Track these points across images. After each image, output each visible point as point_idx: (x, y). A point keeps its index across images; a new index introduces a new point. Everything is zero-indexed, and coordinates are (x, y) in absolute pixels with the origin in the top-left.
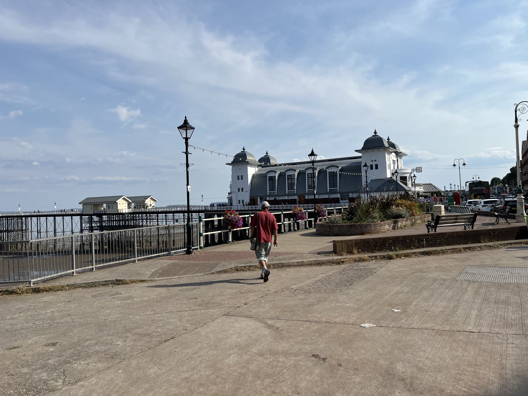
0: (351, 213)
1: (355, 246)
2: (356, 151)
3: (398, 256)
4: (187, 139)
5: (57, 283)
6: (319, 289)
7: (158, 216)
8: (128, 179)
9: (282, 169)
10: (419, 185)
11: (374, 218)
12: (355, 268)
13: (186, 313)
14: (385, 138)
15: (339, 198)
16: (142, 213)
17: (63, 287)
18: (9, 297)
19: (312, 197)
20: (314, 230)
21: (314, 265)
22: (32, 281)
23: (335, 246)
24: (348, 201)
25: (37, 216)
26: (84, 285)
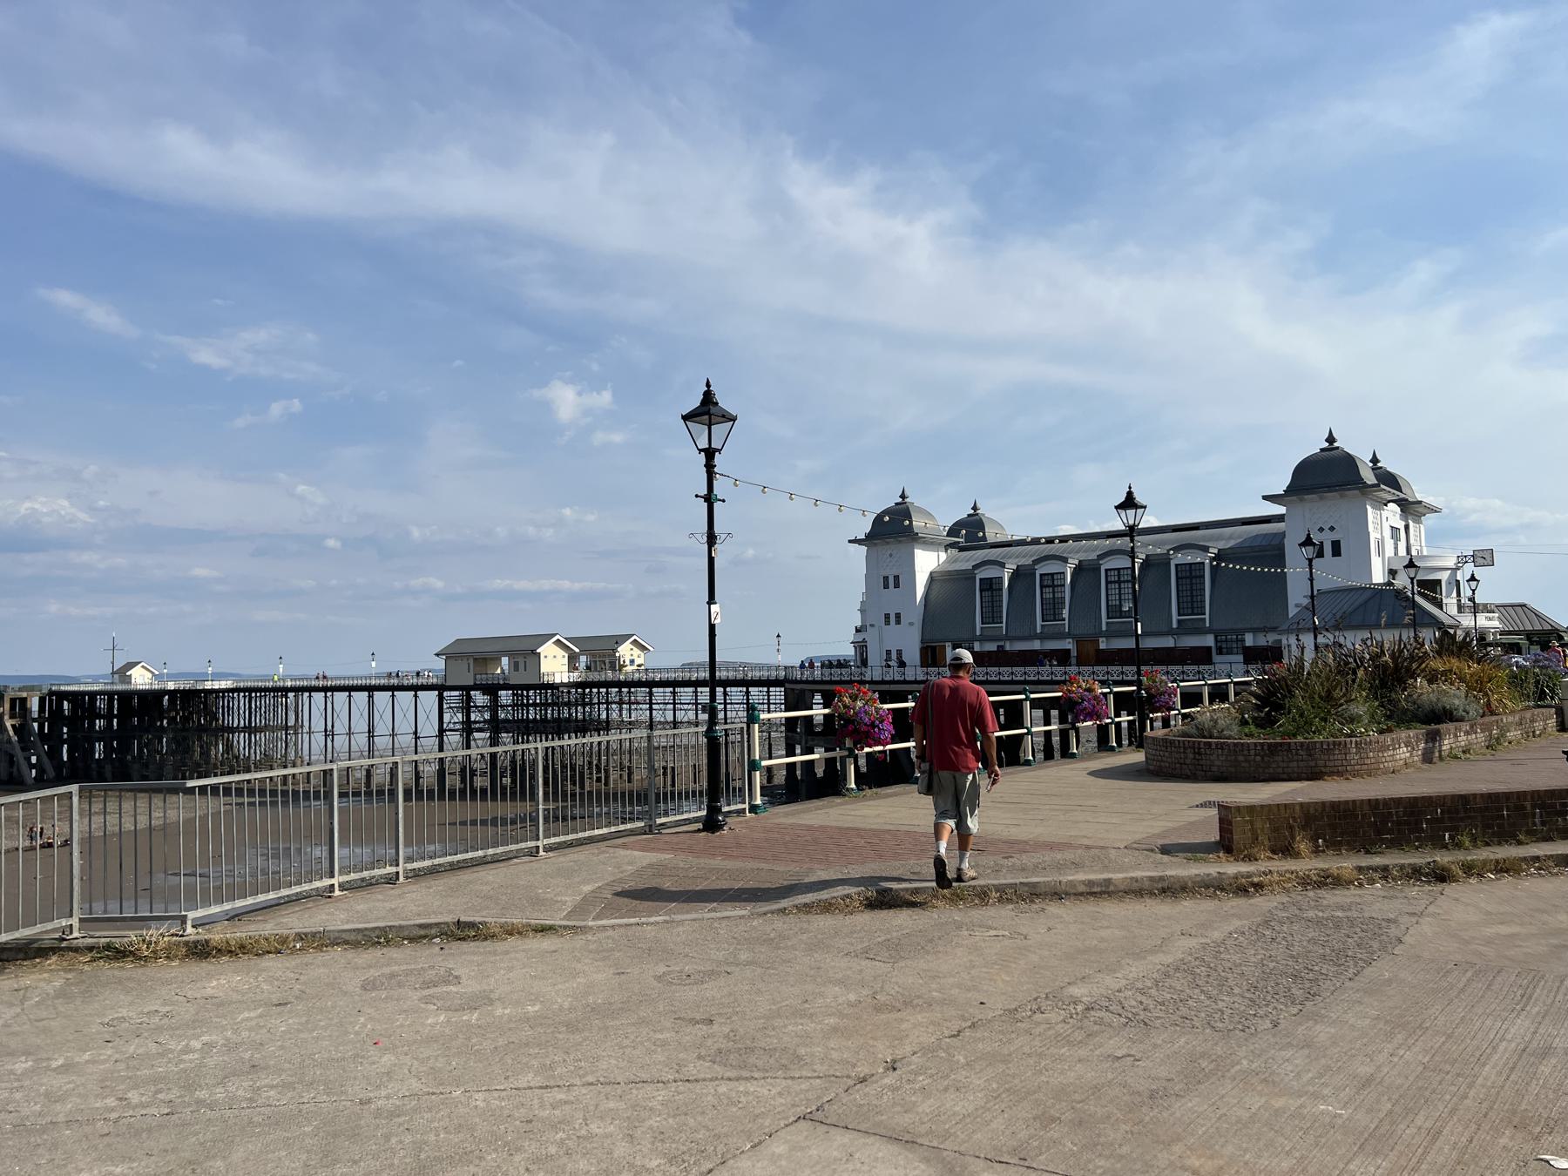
0: (1270, 703)
1: (1303, 828)
2: (1265, 498)
3: (1469, 869)
4: (710, 453)
5: (267, 927)
6: (1184, 1011)
7: (651, 694)
8: (577, 586)
9: (1024, 557)
10: (1487, 609)
11: (1352, 720)
12: (1311, 914)
13: (662, 1094)
14: (1363, 456)
16: (608, 684)
17: (284, 940)
18: (109, 970)
19: (1129, 643)
20: (1138, 757)
21: (1151, 894)
22: (191, 915)
23: (1225, 824)
24: (1240, 658)
25: (325, 689)
26: (352, 937)
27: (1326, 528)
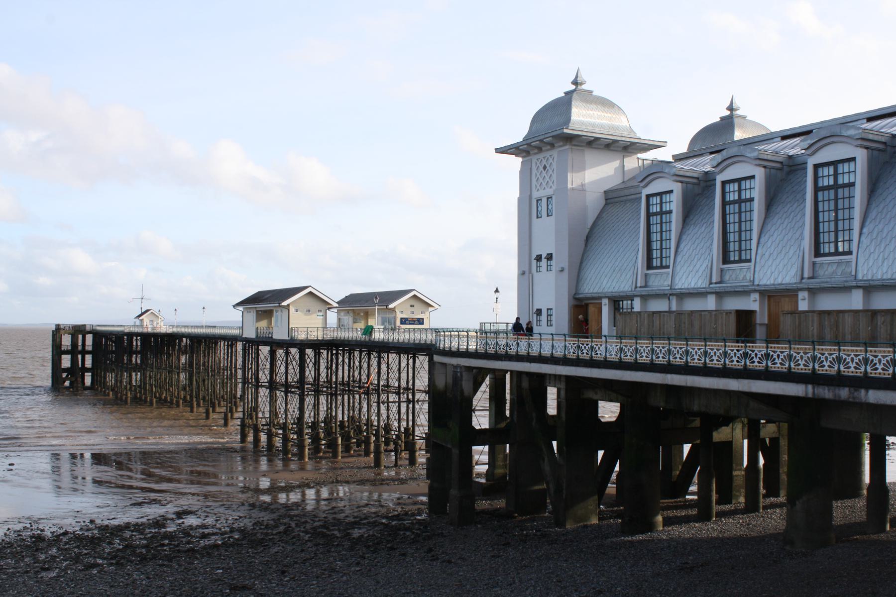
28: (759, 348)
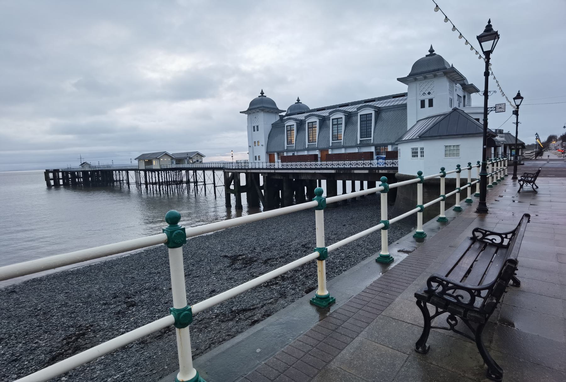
2: (398, 79)
4: (487, 54)
15: (372, 153)
27: (427, 92)
28: (319, 163)
